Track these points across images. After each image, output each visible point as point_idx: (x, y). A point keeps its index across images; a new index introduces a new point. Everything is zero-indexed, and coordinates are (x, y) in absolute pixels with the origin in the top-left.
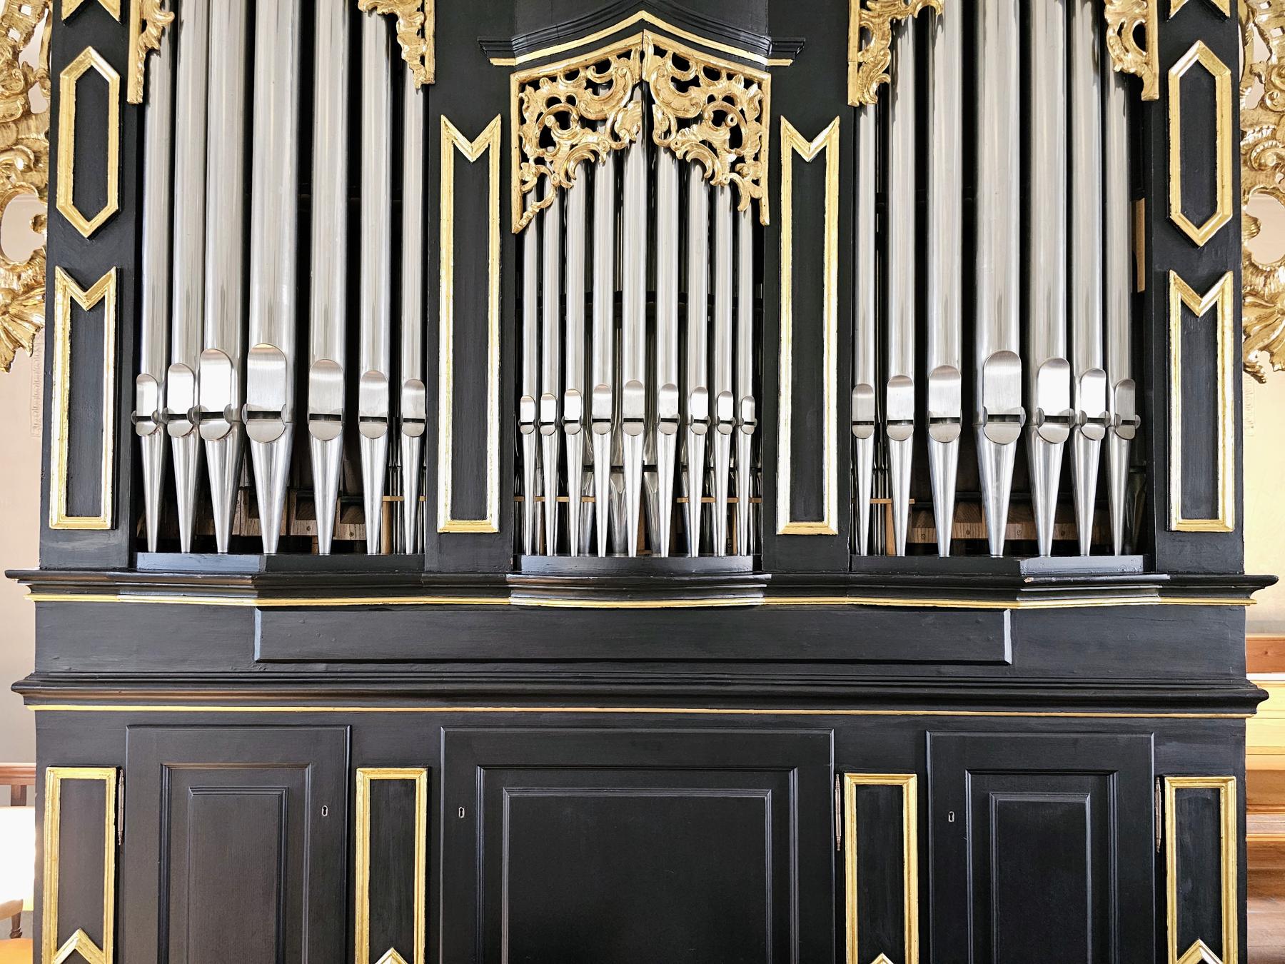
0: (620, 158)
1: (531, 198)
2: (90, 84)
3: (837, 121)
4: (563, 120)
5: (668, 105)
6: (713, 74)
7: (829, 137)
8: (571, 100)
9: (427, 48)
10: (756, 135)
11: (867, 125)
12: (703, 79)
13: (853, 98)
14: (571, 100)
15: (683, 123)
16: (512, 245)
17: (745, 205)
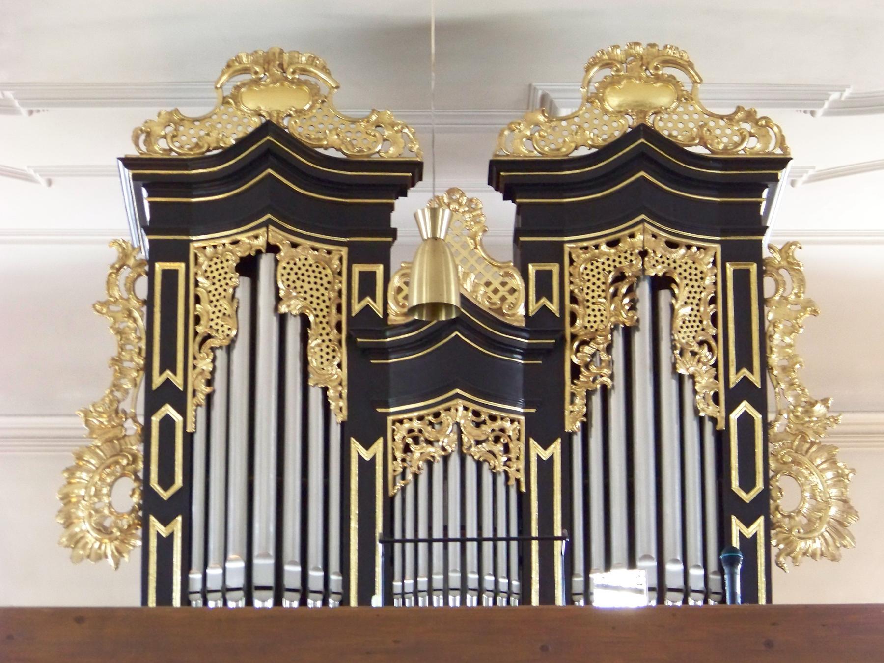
0: (446, 459)
1: (398, 478)
2: (167, 424)
3: (559, 440)
4: (416, 440)
5: (470, 433)
6: (493, 418)
7: (555, 448)
8: (420, 431)
9: (343, 403)
10: (518, 447)
11: (577, 441)
12: (488, 421)
13: (568, 428)
14: (420, 431)
15: (478, 442)
16: (389, 502)
17: (512, 482)
